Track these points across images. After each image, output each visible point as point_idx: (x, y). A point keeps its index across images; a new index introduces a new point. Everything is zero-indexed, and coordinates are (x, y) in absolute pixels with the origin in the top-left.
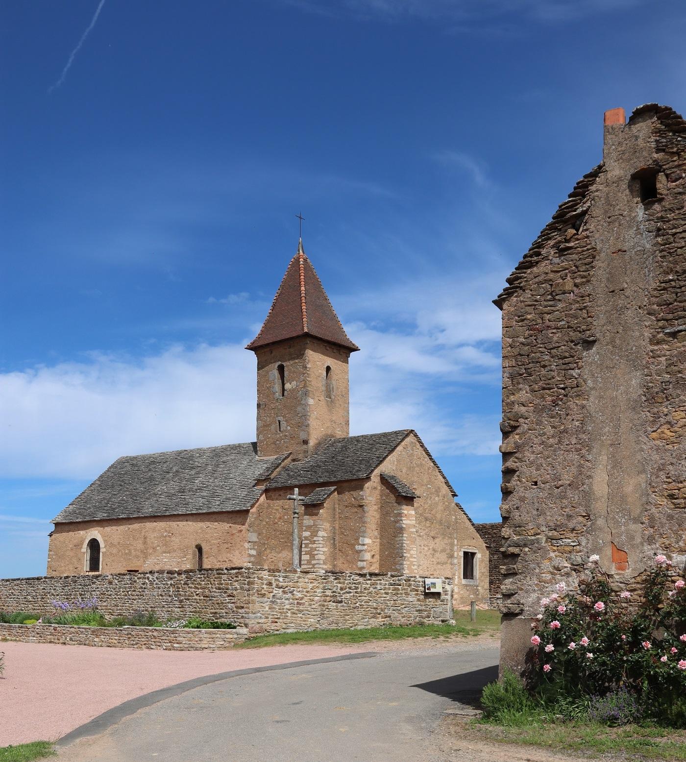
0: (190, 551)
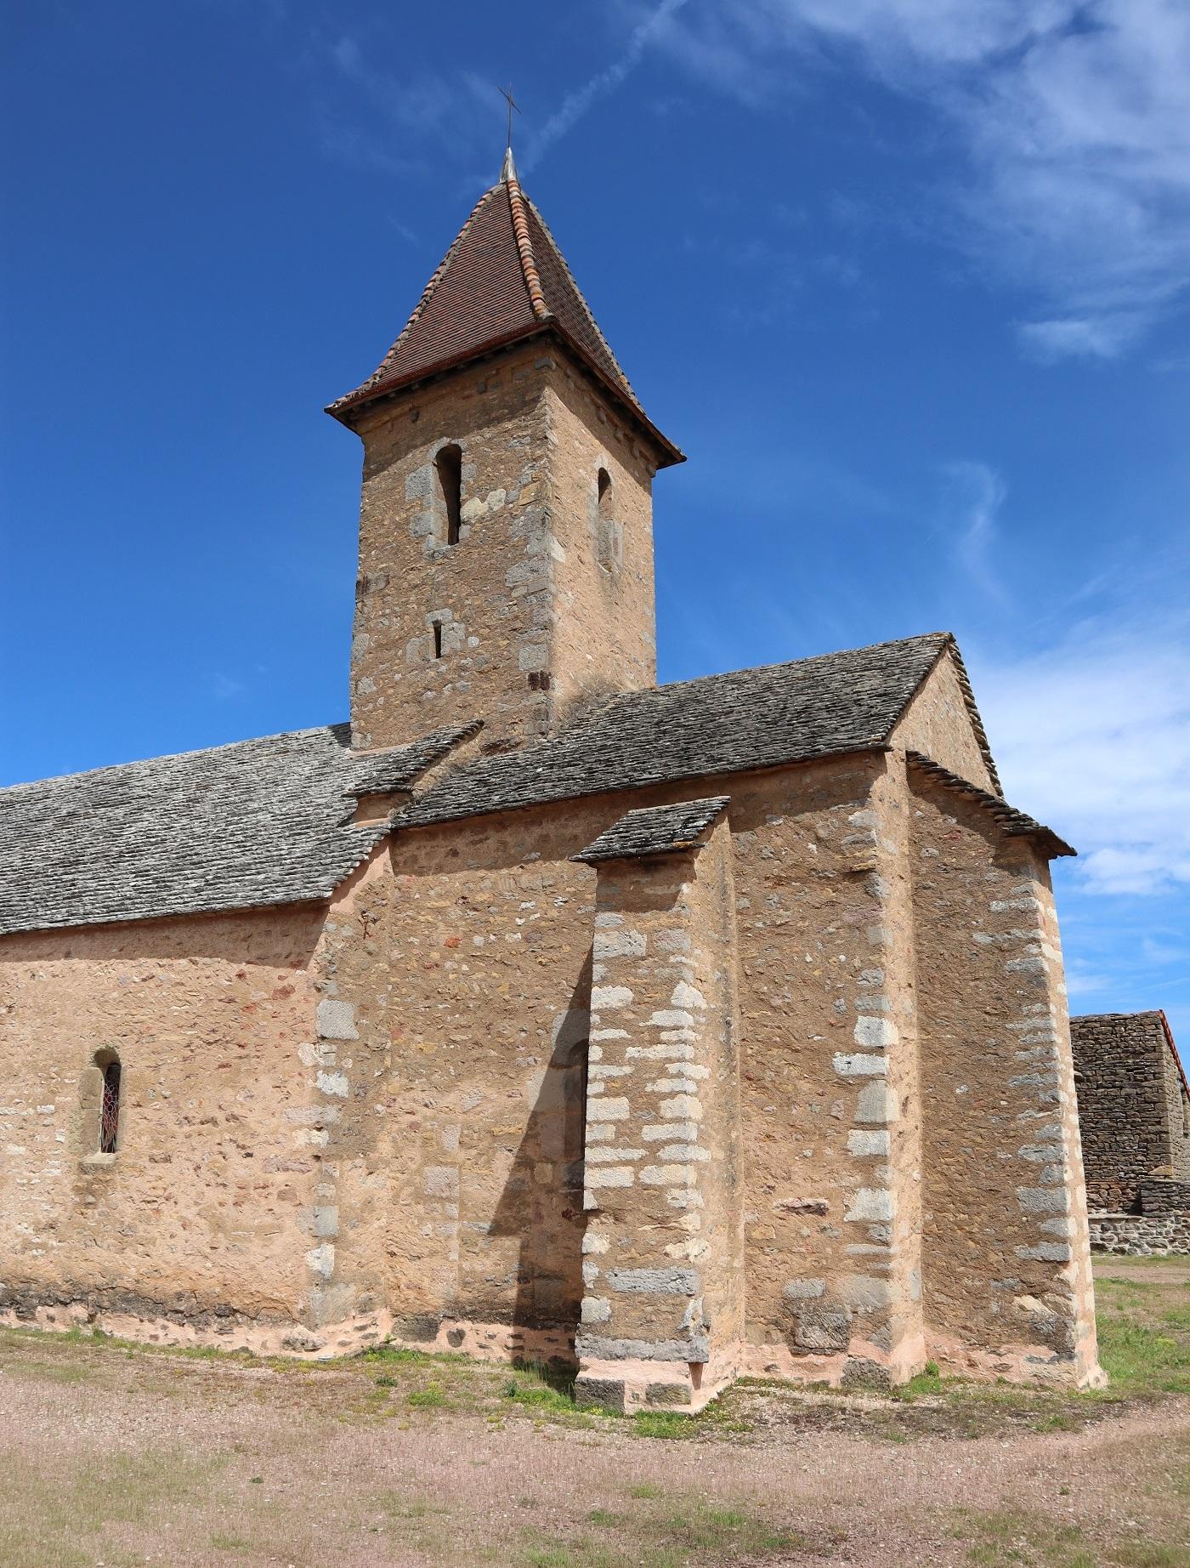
0: (73, 1077)
